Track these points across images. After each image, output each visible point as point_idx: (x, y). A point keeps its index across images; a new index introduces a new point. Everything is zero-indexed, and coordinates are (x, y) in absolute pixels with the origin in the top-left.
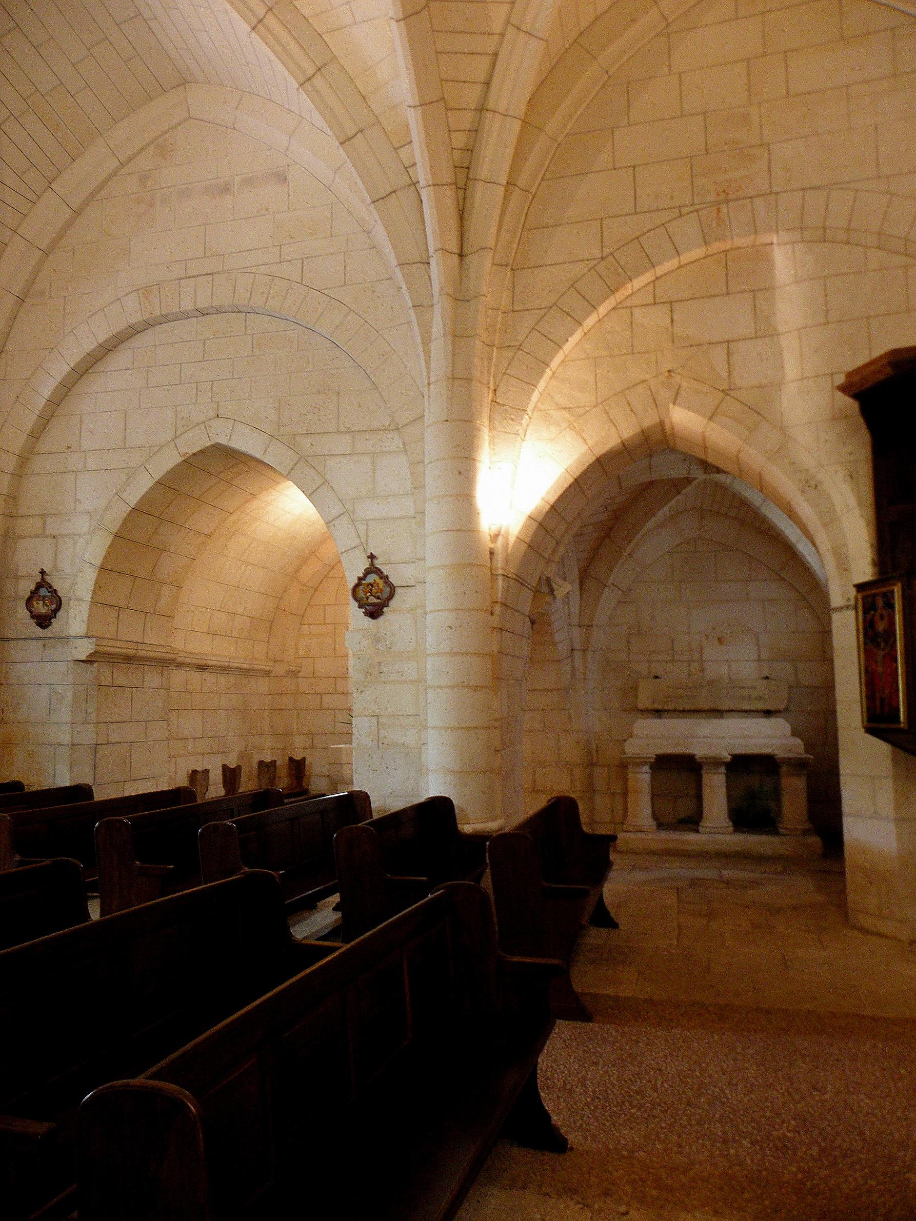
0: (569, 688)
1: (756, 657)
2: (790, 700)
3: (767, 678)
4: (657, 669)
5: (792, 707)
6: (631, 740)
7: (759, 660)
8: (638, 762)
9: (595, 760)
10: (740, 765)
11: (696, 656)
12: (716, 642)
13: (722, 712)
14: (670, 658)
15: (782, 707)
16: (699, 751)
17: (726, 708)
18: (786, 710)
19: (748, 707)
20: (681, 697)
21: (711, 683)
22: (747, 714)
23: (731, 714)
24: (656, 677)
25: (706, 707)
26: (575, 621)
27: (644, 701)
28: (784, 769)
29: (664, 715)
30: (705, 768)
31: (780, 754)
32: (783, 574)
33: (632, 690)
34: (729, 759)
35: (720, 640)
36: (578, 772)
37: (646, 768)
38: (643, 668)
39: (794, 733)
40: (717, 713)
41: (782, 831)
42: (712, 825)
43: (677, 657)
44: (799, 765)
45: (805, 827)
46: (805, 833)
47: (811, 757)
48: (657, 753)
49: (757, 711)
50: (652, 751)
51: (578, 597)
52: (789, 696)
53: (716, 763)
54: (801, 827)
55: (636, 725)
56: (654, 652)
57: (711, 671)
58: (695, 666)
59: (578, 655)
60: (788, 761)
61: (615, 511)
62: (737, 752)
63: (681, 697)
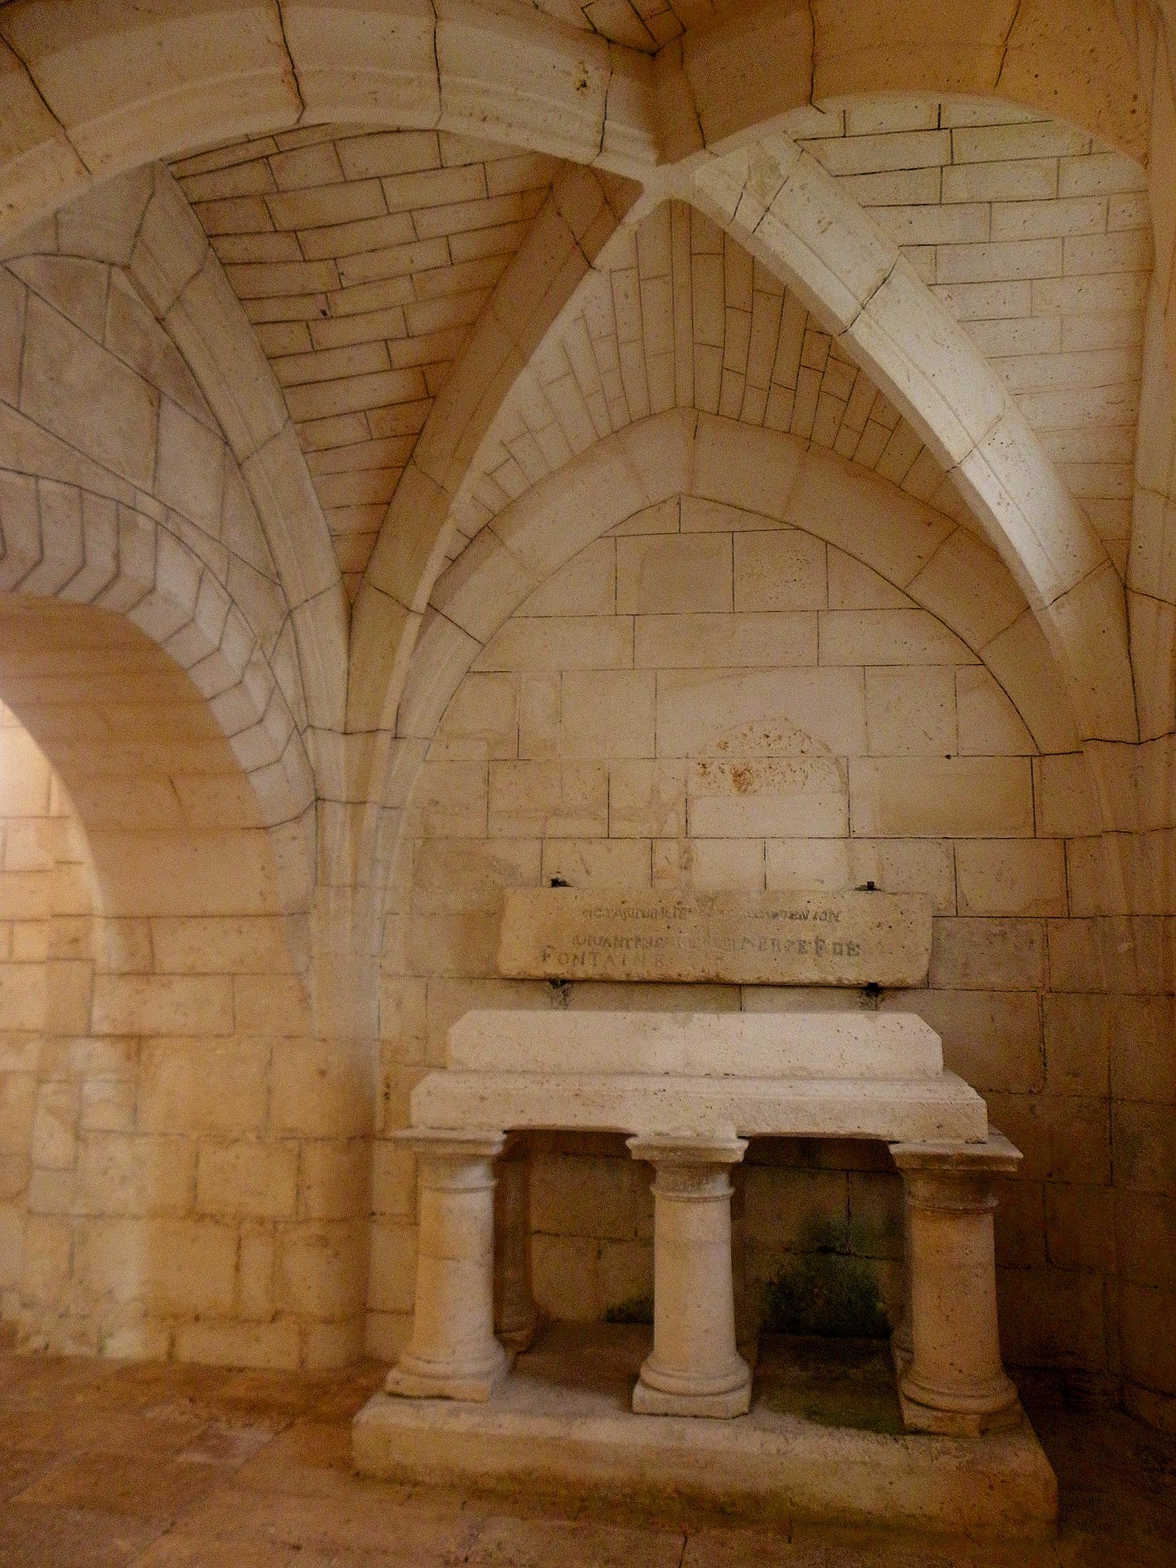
0: (305, 913)
1: (841, 830)
2: (935, 954)
3: (871, 887)
4: (561, 860)
5: (942, 976)
6: (434, 1079)
7: (849, 836)
8: (443, 1155)
9: (379, 1124)
10: (776, 1158)
11: (672, 826)
12: (728, 782)
13: (740, 986)
14: (601, 830)
15: (912, 974)
16: (644, 1122)
17: (750, 977)
18: (927, 984)
19: (811, 975)
20: (621, 942)
21: (709, 901)
22: (812, 995)
23: (765, 993)
24: (555, 883)
25: (691, 972)
26: (329, 712)
27: (517, 956)
28: (921, 1189)
29: (577, 993)
30: (662, 1177)
31: (909, 1140)
32: (920, 592)
33: (485, 921)
34: (737, 1150)
35: (740, 778)
36: (318, 1163)
37: (478, 1177)
38: (525, 858)
39: (956, 1061)
40: (726, 991)
41: (912, 1415)
42: (675, 1384)
43: (619, 828)
44: (971, 1180)
45: (989, 1404)
46: (989, 1425)
47: (1017, 1154)
48: (508, 1125)
49: (840, 986)
50: (491, 1127)
51: (344, 656)
52: (935, 941)
53: (696, 1165)
54: (973, 1404)
55: (456, 1031)
56: (556, 812)
57: (715, 866)
58: (668, 852)
59: (336, 815)
60: (929, 1164)
61: (421, 368)
62: (766, 1128)
63: (621, 942)
